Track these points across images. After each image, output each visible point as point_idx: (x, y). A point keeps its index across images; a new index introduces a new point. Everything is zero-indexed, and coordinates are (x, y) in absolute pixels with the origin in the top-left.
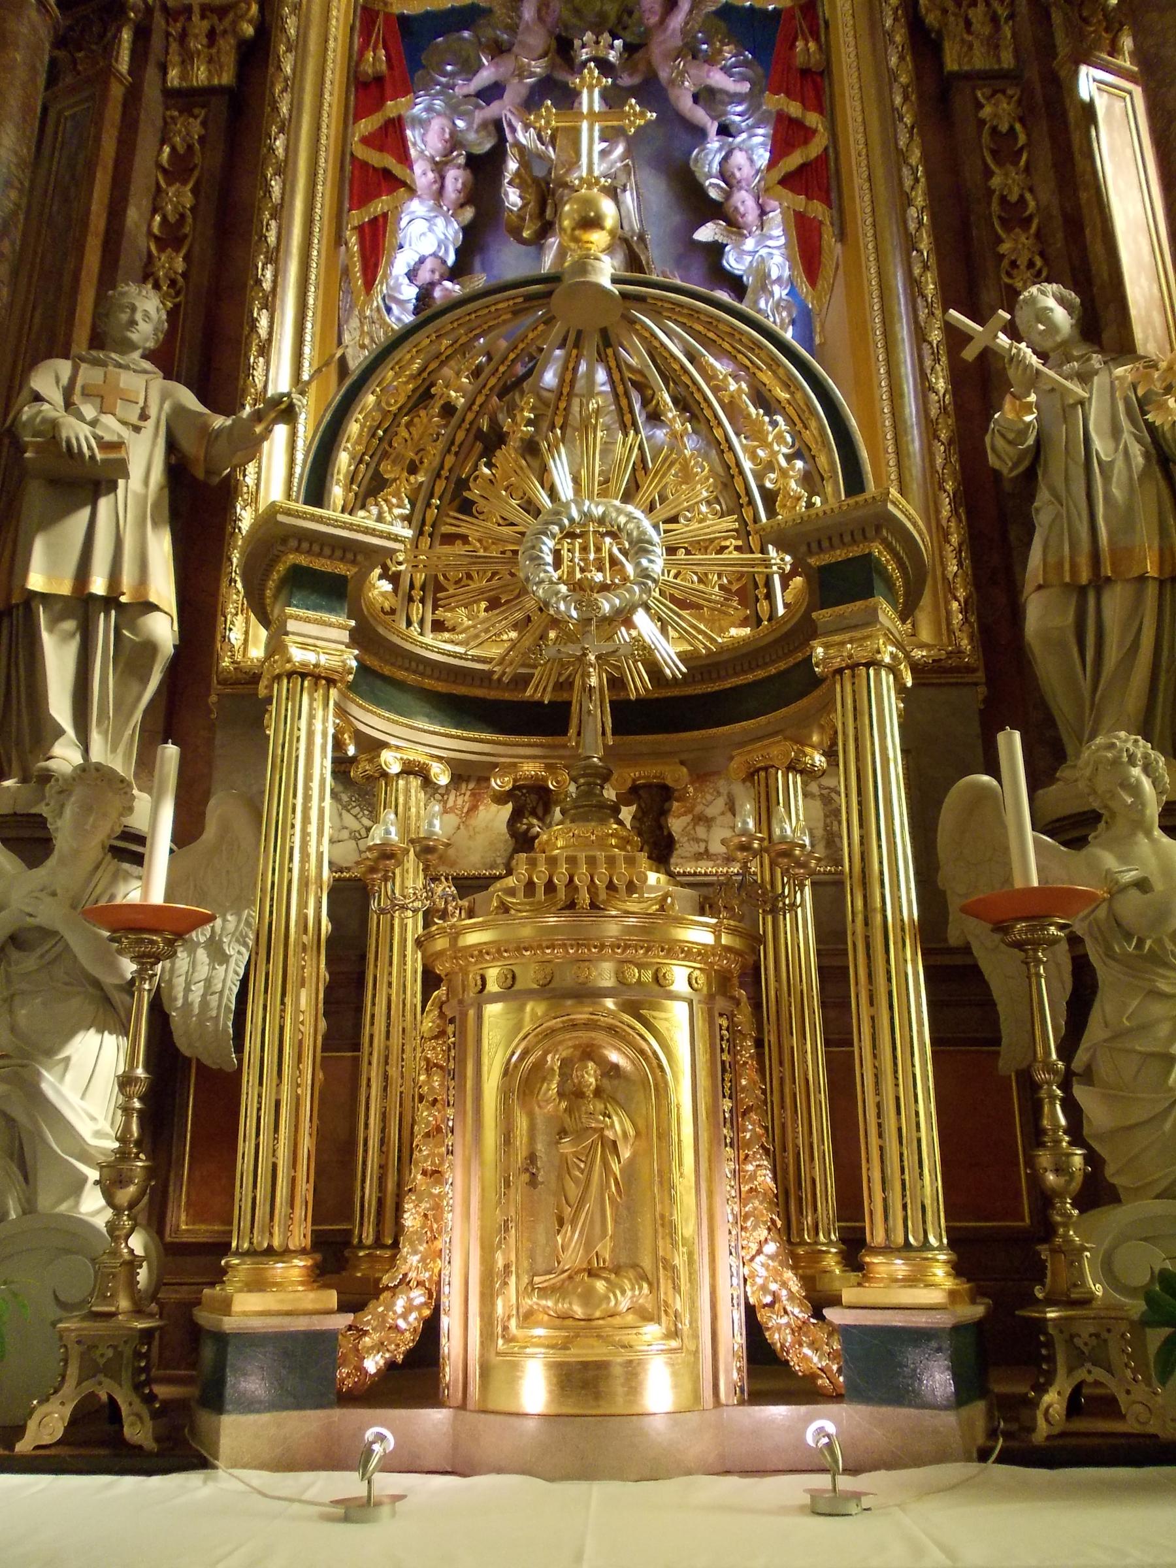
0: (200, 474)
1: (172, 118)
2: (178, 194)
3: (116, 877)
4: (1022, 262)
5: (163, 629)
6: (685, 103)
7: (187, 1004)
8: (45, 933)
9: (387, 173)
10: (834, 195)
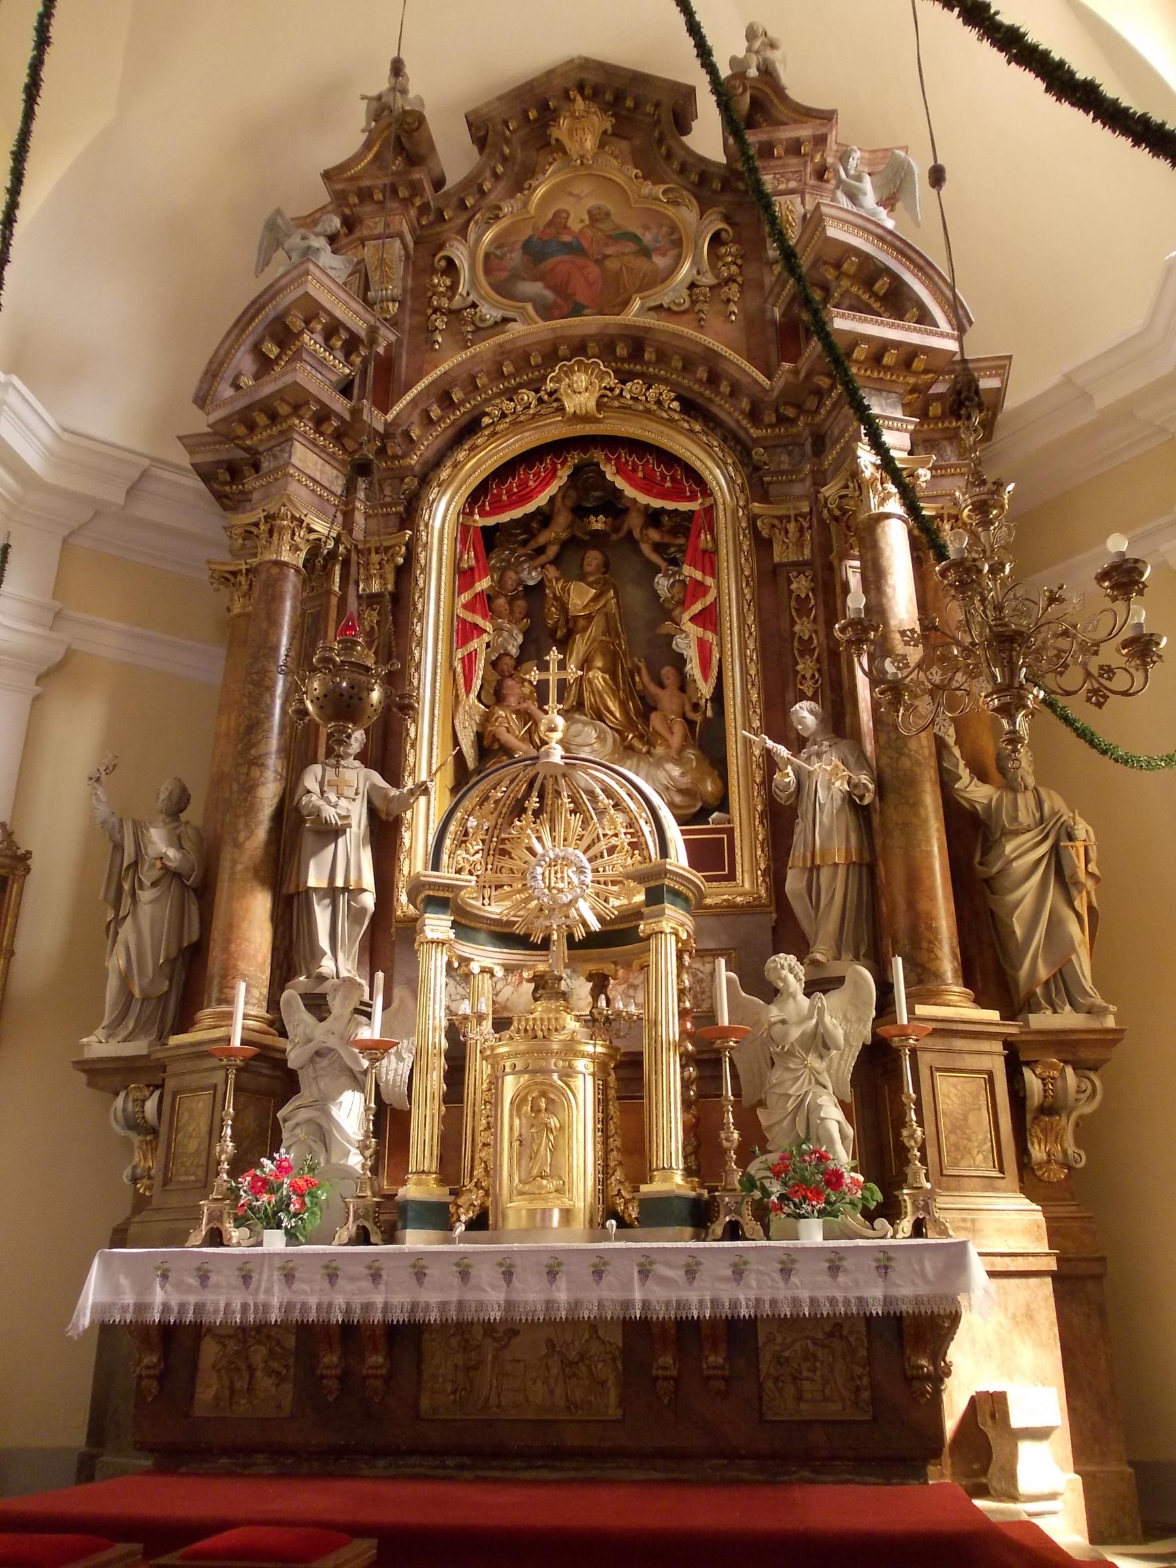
0: (384, 817)
3: (359, 1024)
4: (808, 676)
5: (369, 900)
7: (387, 1080)
8: (331, 1050)
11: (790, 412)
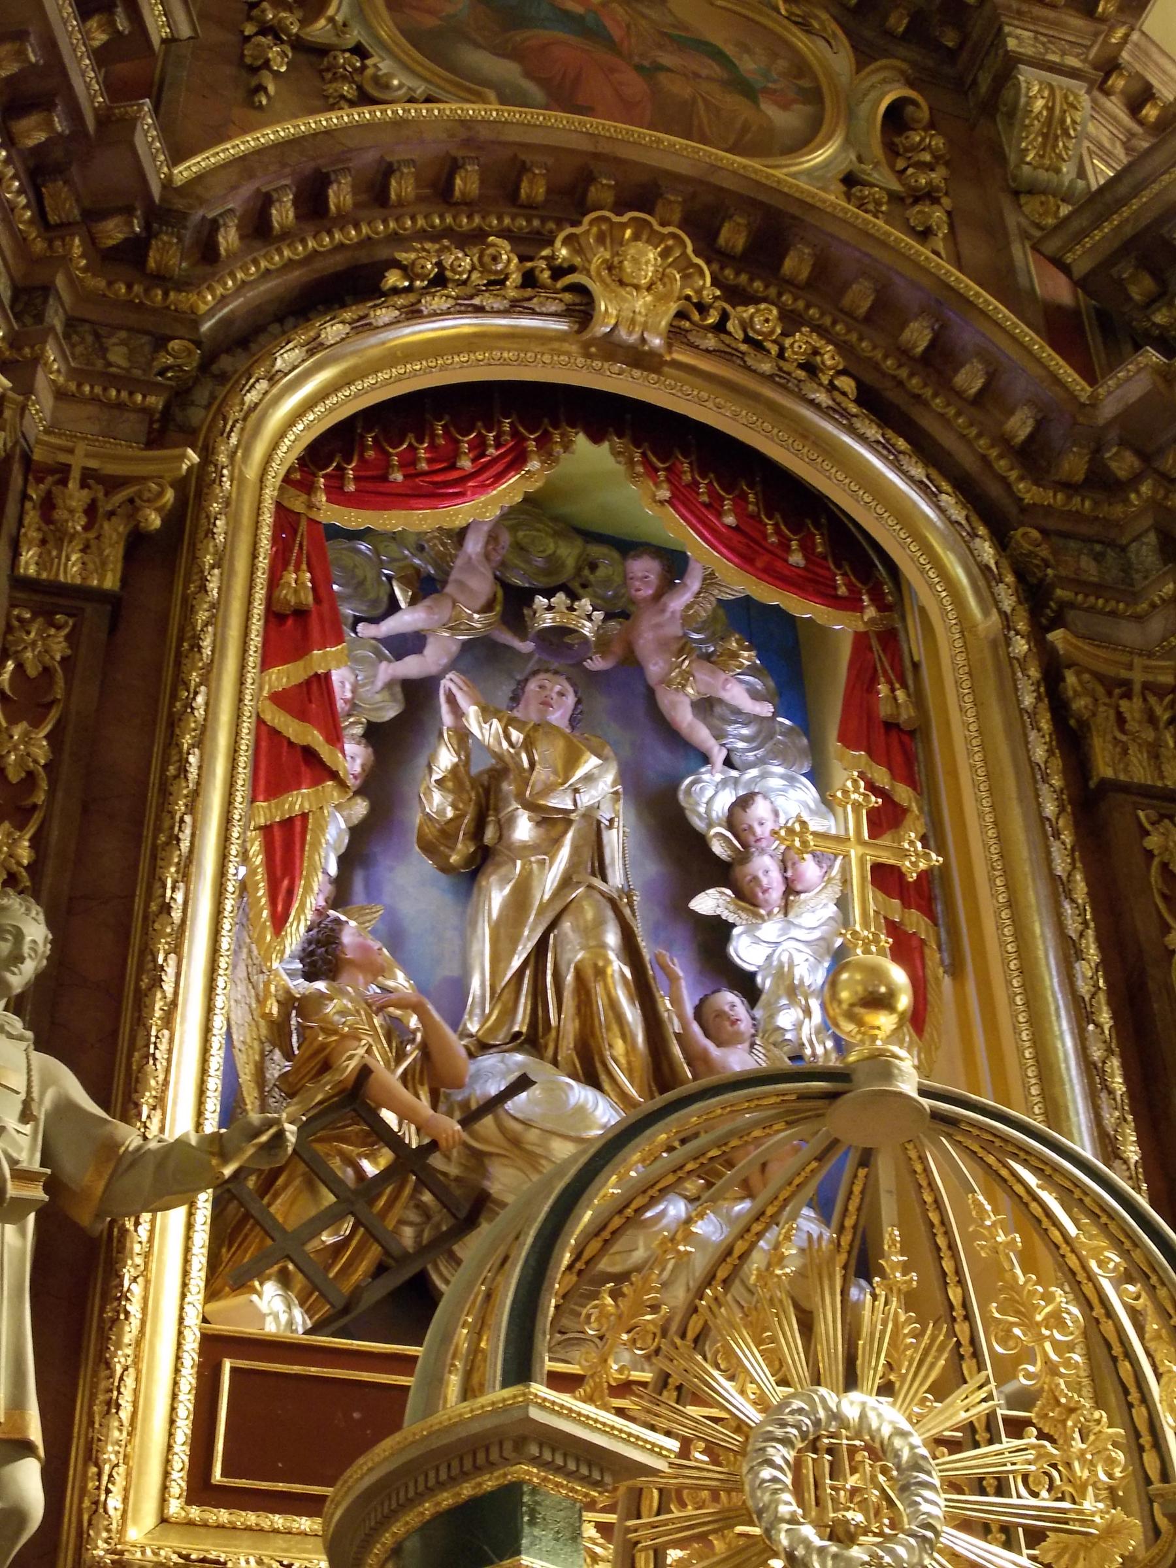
1: (20, 619)
2: (27, 739)
6: (684, 717)
9: (309, 755)
10: (939, 908)
11: (1122, 464)
